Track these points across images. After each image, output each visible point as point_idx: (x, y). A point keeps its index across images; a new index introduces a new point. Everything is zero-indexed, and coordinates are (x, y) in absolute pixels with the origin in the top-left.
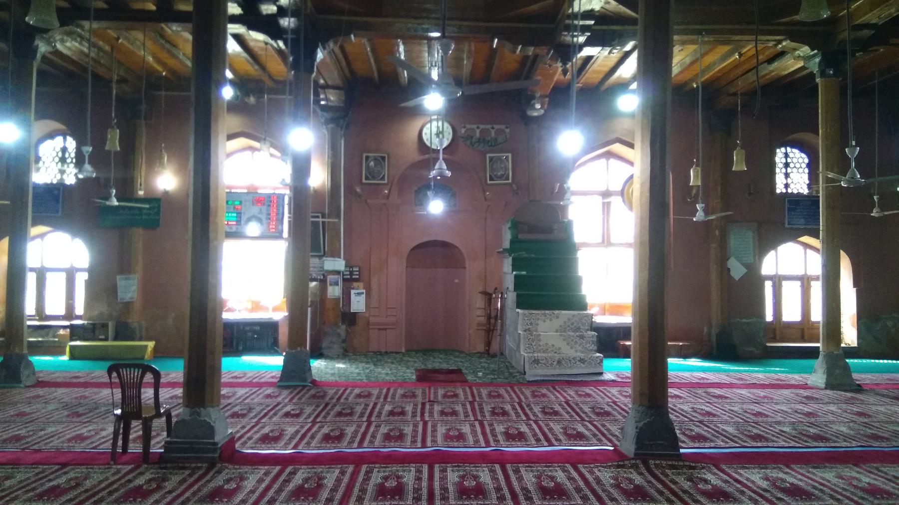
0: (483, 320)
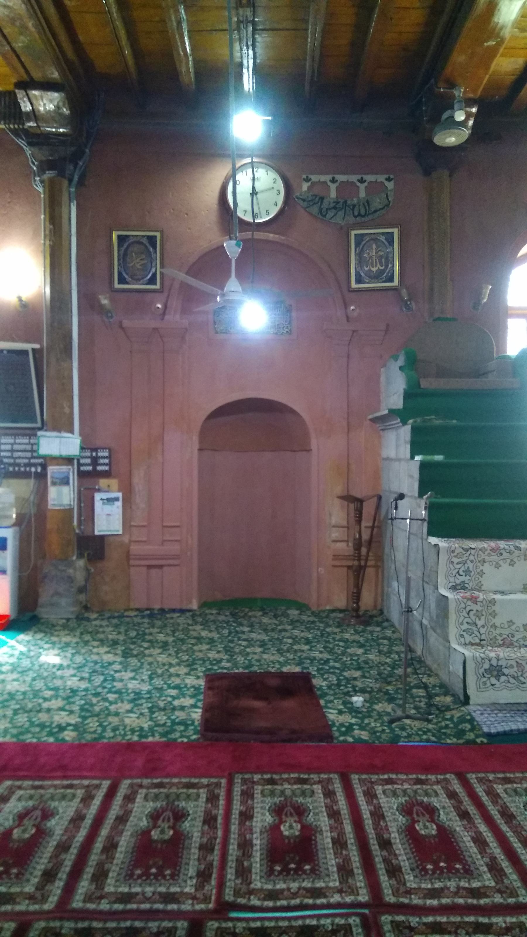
0: (345, 548)
